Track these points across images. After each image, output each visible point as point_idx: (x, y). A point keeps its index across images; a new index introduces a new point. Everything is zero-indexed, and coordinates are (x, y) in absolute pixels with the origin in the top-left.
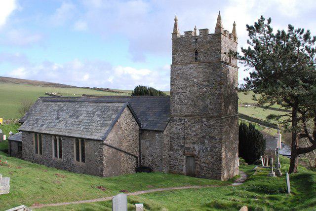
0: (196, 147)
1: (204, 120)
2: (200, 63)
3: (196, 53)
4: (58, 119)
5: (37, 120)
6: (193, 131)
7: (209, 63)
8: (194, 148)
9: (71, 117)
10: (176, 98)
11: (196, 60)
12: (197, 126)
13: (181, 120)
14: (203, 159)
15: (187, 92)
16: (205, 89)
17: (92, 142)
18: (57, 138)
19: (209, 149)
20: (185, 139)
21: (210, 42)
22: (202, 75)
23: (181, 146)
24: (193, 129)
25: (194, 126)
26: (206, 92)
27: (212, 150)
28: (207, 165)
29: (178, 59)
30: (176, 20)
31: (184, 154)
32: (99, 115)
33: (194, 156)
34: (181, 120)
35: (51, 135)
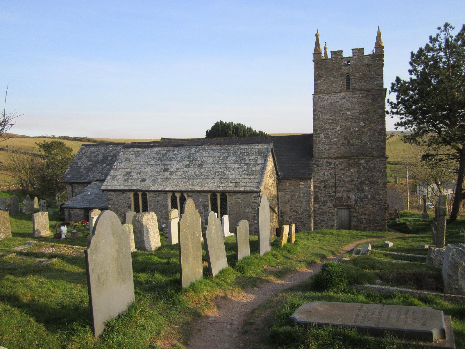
0: (352, 196)
1: (362, 161)
2: (354, 90)
3: (348, 79)
4: (166, 170)
5: (128, 173)
6: (347, 176)
7: (368, 90)
8: (349, 197)
9: (188, 166)
10: (322, 136)
11: (348, 88)
12: (352, 170)
13: (330, 163)
14: (362, 210)
15: (338, 128)
16: (362, 124)
17: (239, 196)
18: (178, 195)
19: (369, 196)
20: (335, 186)
21: (367, 66)
22: (357, 106)
23: (331, 196)
24: (348, 174)
25: (349, 170)
26: (363, 127)
27: (373, 198)
28: (367, 217)
29: (323, 87)
30: (317, 36)
31: (335, 206)
32: (236, 161)
33: (349, 207)
34: (330, 163)
35: (165, 192)
